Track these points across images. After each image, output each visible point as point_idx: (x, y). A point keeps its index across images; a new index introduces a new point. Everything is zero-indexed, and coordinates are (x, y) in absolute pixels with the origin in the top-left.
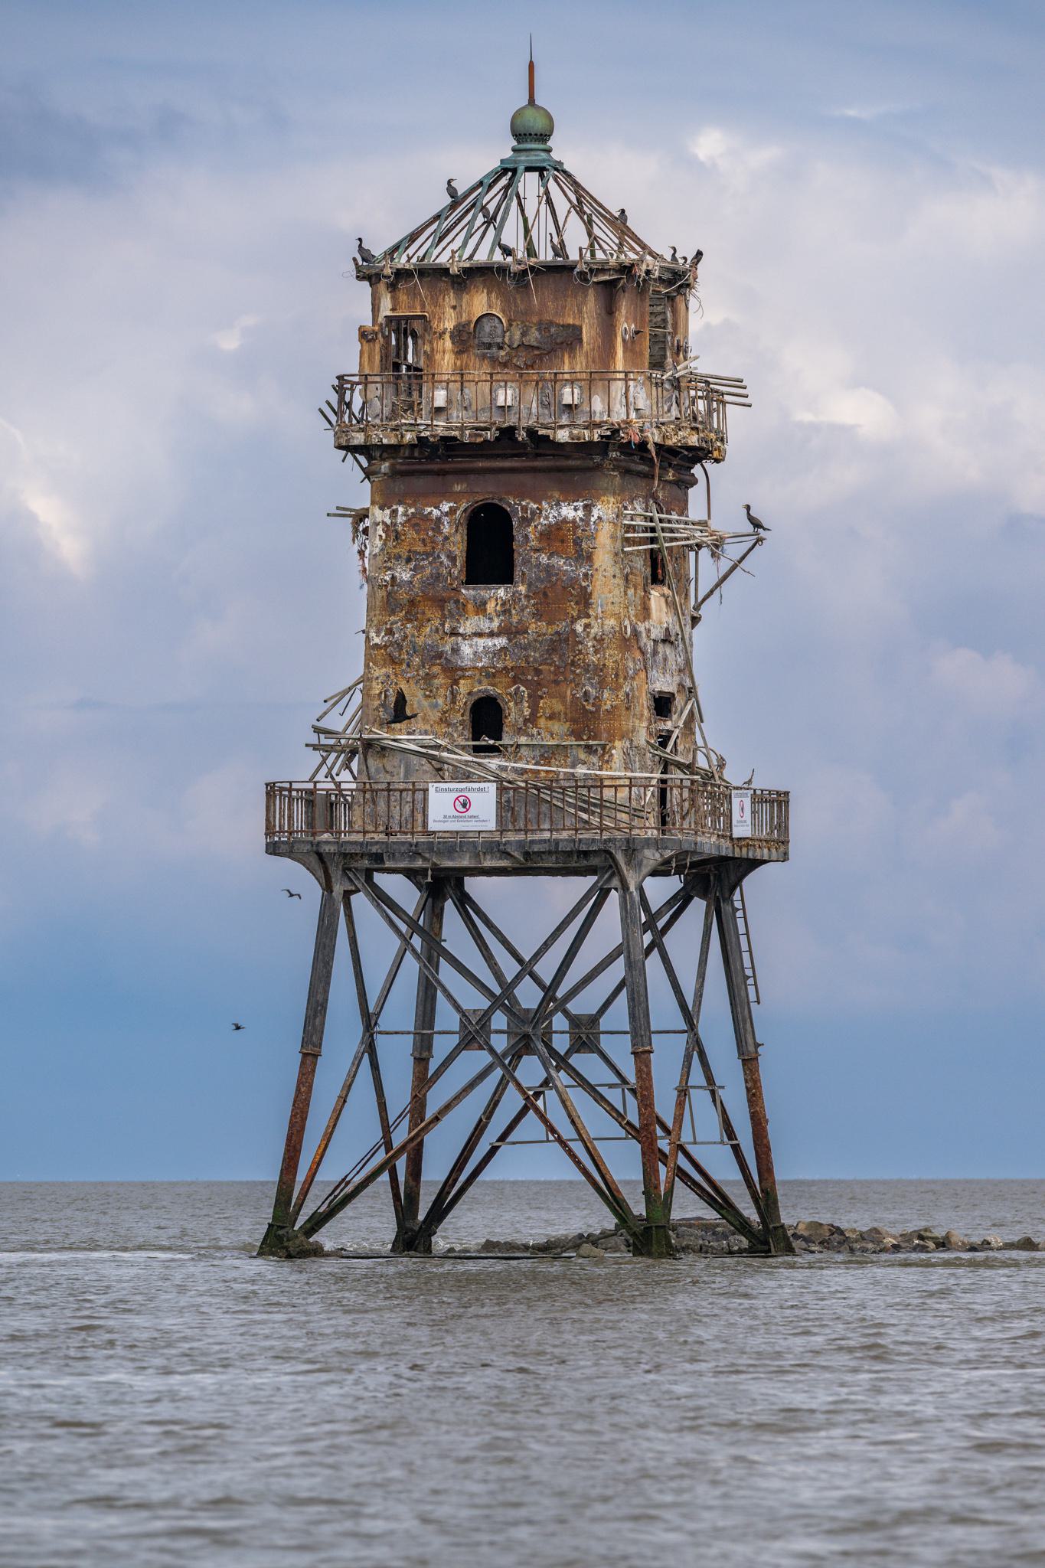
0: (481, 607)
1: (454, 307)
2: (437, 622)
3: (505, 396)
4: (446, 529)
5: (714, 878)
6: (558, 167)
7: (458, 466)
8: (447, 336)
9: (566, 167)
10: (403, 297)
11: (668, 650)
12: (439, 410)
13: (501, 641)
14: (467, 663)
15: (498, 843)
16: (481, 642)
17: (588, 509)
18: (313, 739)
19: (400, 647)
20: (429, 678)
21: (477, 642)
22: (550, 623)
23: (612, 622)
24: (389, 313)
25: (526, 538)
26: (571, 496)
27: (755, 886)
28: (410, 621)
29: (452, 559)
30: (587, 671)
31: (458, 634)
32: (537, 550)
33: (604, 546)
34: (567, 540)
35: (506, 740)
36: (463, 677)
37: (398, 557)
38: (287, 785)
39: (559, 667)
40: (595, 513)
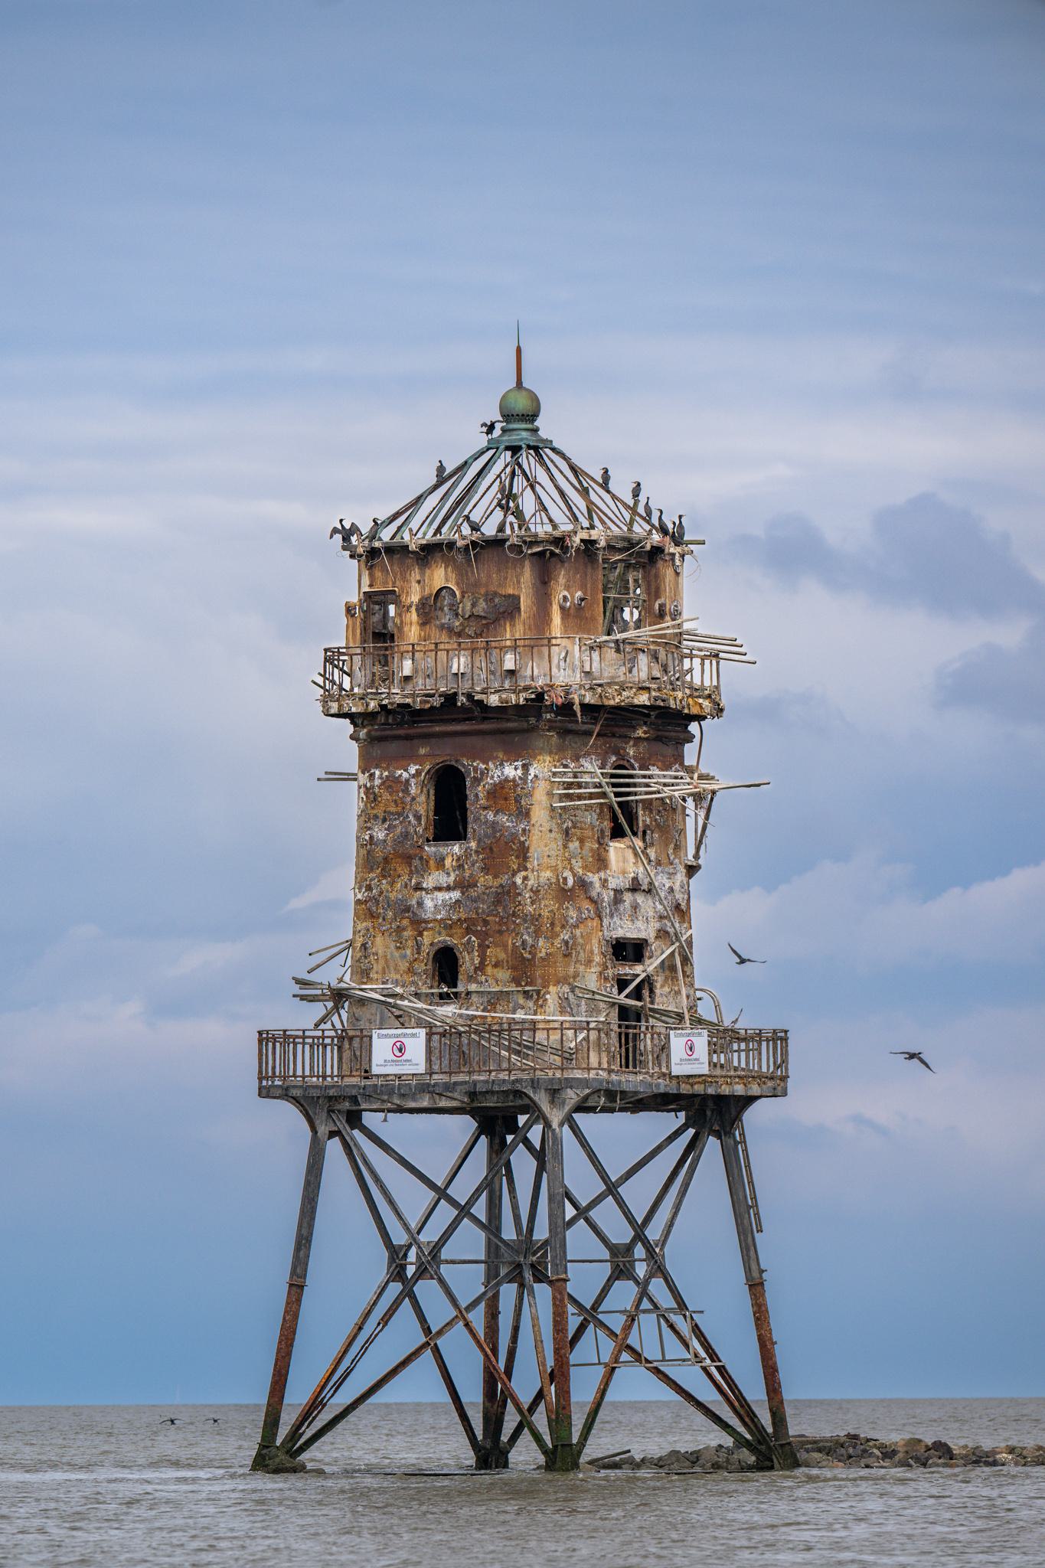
0: (440, 863)
1: (419, 582)
2: (406, 878)
3: (460, 663)
4: (413, 790)
5: (713, 1113)
6: (548, 444)
7: (425, 730)
8: (413, 609)
9: (555, 445)
10: (378, 574)
11: (640, 898)
12: (407, 679)
13: (456, 895)
14: (429, 916)
15: (428, 1085)
16: (441, 896)
17: (525, 767)
18: (297, 989)
19: (377, 902)
20: (400, 930)
21: (436, 901)
22: (495, 877)
23: (548, 874)
24: (367, 589)
25: (477, 795)
26: (512, 755)
27: (755, 1117)
28: (384, 877)
29: (418, 818)
30: (525, 921)
31: (422, 889)
32: (485, 808)
33: (540, 803)
34: (505, 795)
35: (460, 988)
36: (426, 929)
37: (376, 817)
38: (300, 1033)
39: (502, 918)
40: (532, 772)
